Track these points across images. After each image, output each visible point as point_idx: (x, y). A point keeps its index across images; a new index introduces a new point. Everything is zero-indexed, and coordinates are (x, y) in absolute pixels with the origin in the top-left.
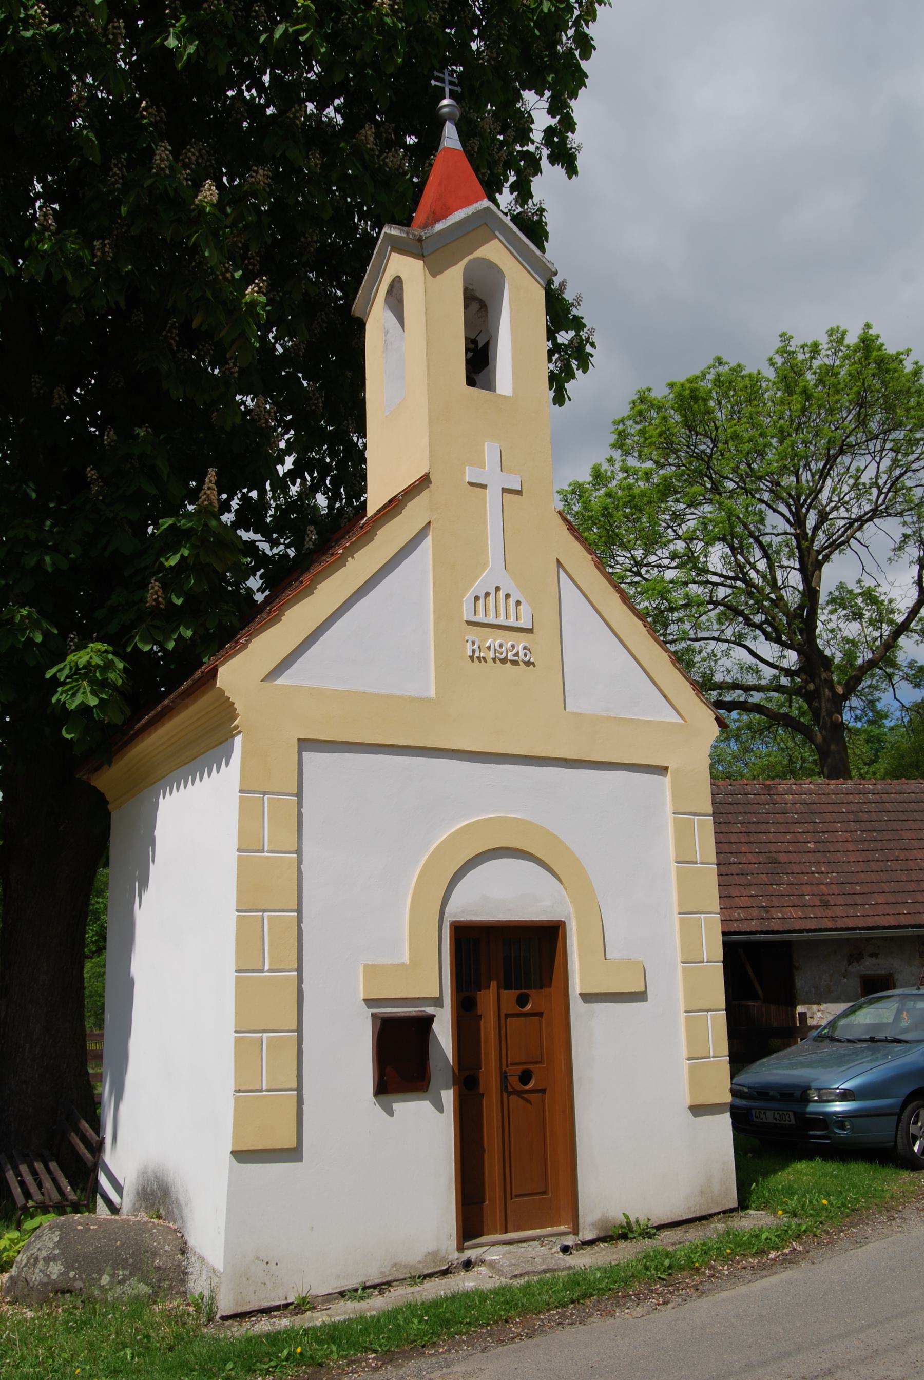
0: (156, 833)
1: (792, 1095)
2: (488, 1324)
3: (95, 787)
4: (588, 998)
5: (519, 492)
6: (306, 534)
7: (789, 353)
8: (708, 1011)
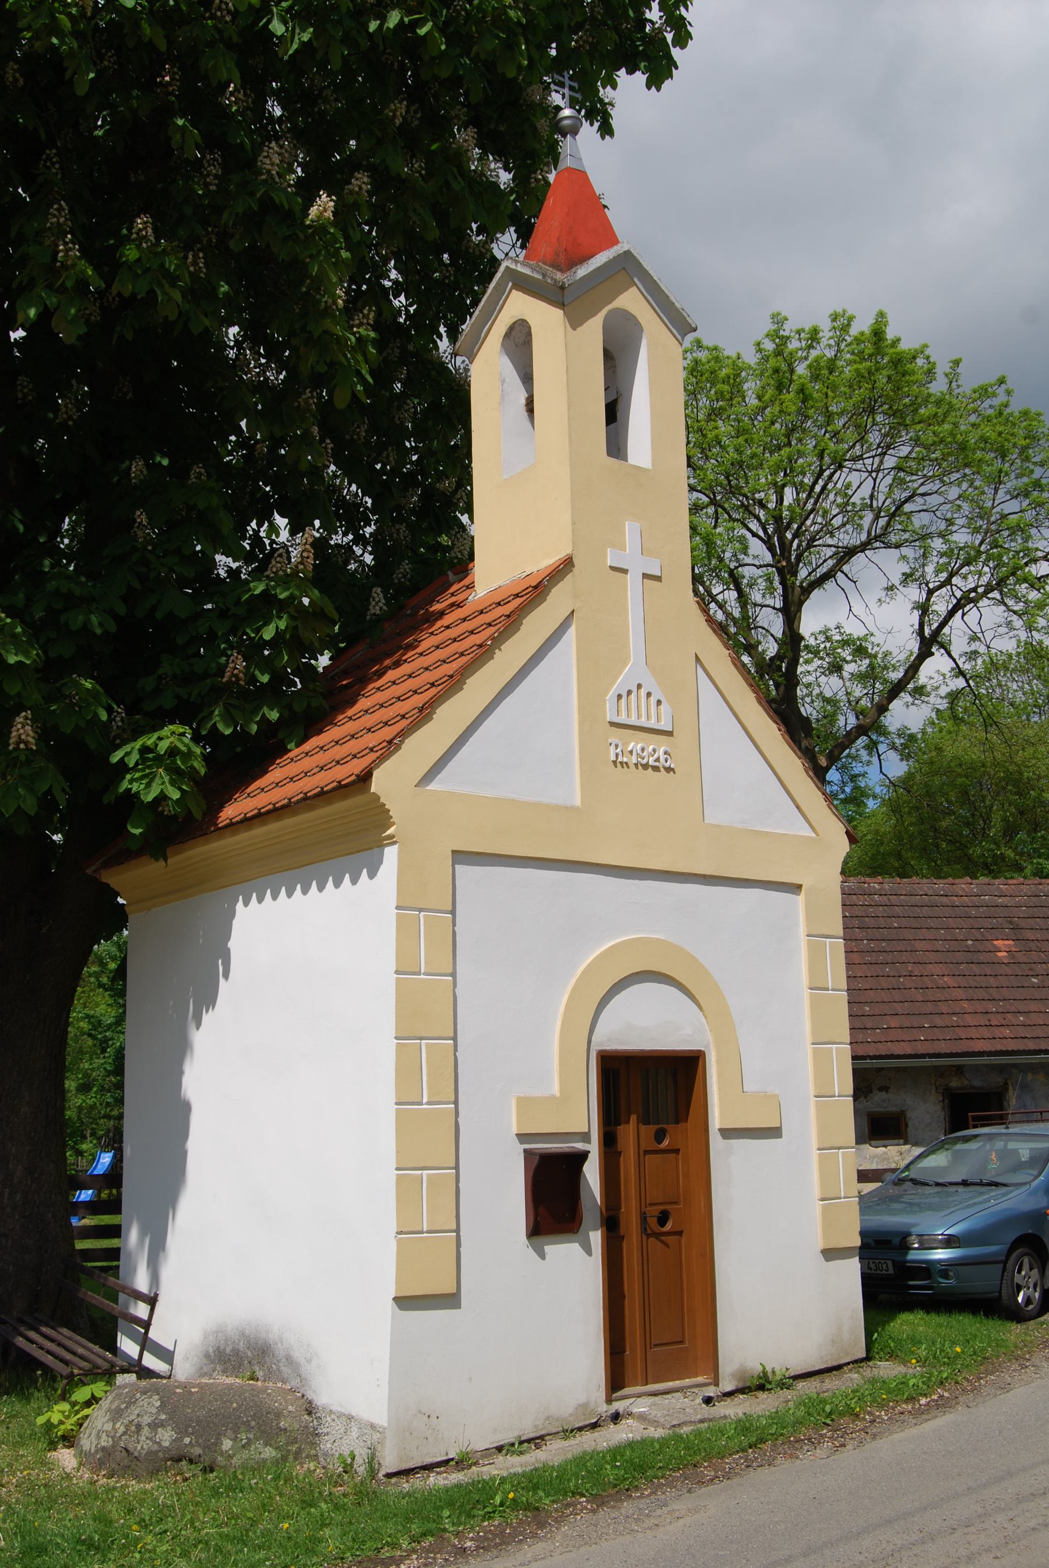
0: (230, 944)
1: (889, 1242)
2: (679, 1469)
3: (108, 885)
4: (728, 1133)
5: (658, 579)
6: (371, 596)
7: (782, 338)
8: (839, 1148)
